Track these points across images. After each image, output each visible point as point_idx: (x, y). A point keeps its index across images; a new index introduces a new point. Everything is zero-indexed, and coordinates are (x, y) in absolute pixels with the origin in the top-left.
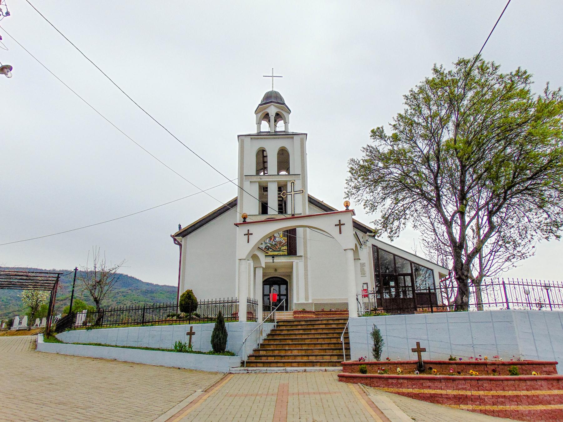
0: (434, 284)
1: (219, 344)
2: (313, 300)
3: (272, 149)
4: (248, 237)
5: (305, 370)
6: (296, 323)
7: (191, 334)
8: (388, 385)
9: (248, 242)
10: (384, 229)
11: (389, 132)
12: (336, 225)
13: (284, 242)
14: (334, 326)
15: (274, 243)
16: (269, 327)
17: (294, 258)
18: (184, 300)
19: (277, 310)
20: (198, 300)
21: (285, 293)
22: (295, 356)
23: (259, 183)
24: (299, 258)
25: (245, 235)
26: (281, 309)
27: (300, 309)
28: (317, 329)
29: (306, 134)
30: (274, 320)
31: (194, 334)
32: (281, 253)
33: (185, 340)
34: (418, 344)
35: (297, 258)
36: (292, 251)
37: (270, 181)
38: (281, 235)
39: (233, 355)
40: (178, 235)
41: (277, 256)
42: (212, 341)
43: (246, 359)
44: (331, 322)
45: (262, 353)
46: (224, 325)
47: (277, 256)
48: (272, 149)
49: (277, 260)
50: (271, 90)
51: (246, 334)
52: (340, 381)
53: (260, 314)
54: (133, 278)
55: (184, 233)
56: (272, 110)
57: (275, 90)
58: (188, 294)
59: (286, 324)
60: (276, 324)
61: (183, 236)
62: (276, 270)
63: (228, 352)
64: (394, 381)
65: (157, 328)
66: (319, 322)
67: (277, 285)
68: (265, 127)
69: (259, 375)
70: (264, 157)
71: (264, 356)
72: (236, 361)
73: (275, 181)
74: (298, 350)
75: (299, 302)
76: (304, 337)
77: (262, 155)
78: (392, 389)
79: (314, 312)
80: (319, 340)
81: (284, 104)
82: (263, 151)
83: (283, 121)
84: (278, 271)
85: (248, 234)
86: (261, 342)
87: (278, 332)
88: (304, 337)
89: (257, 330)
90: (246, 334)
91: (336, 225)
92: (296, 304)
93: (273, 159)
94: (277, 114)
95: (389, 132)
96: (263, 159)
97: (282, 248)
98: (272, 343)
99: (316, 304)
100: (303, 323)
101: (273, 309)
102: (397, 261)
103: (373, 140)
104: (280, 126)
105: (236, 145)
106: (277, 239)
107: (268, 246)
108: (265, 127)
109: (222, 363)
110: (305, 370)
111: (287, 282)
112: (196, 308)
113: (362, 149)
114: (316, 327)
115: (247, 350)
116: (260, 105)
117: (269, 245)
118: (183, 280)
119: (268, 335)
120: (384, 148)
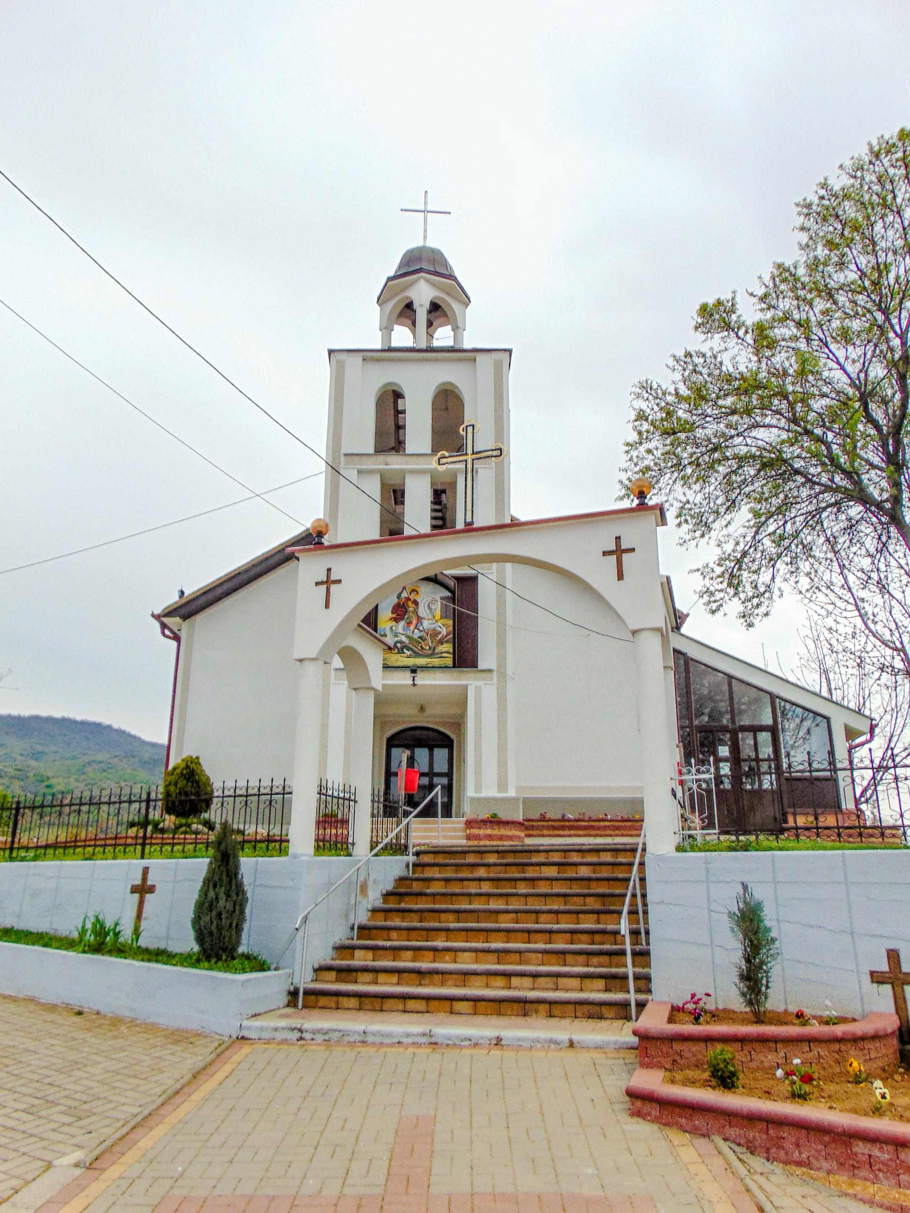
0: (831, 753)
1: (219, 937)
2: (518, 789)
3: (419, 392)
4: (328, 590)
5: (498, 1041)
6: (470, 859)
7: (143, 889)
8: (851, 1165)
9: (327, 606)
10: (731, 591)
11: (749, 313)
12: (605, 553)
13: (444, 632)
14: (584, 871)
15: (417, 634)
16: (393, 868)
17: (472, 675)
18: (176, 784)
19: (417, 816)
20: (217, 784)
21: (445, 769)
22: (466, 974)
23: (383, 476)
24: (484, 675)
25: (317, 584)
26: (429, 812)
27: (485, 815)
28: (533, 880)
29: (510, 351)
30: (406, 847)
31: (151, 889)
32: (436, 661)
33: (120, 912)
34: (893, 956)
35: (480, 675)
36: (464, 656)
37: (413, 472)
38: (438, 614)
39: (262, 967)
40: (170, 613)
41: (425, 668)
42: (196, 921)
43: (304, 980)
44: (575, 858)
45: (361, 959)
46: (237, 866)
47: (425, 668)
48: (419, 392)
49: (423, 679)
50: (420, 243)
51: (307, 900)
52: (637, 1114)
53: (362, 825)
54: (123, 732)
55: (190, 608)
56: (423, 293)
57: (430, 244)
58: (187, 767)
59: (440, 859)
60: (411, 859)
61: (185, 618)
62: (422, 709)
63: (247, 957)
64: (883, 1154)
65: (49, 866)
66: (540, 858)
67: (420, 751)
68: (402, 336)
69: (338, 1051)
70: (398, 412)
71: (366, 970)
72: (270, 987)
73: (423, 472)
74: (476, 951)
75: (483, 795)
76: (494, 905)
77: (391, 399)
78: (872, 1189)
79: (521, 824)
80: (543, 917)
81: (452, 277)
82: (398, 395)
83: (449, 327)
84: (428, 712)
85: (328, 582)
86: (363, 918)
87: (416, 887)
88: (494, 905)
89: (349, 882)
90: (307, 900)
91: (605, 553)
92: (472, 799)
93: (421, 418)
94: (435, 307)
95: (749, 313)
96: (396, 418)
97: (440, 648)
98: (397, 922)
99: (526, 801)
100: (492, 859)
101: (406, 814)
102: (735, 688)
103: (703, 337)
104: (443, 336)
105: (324, 370)
106: (426, 624)
107: (401, 642)
108: (402, 336)
109: (217, 999)
110: (498, 1041)
111: (452, 741)
112: (208, 803)
113: (671, 363)
114: (530, 873)
115: (315, 947)
116: (390, 279)
117: (404, 639)
118: (182, 730)
119: (387, 895)
120: (738, 357)
